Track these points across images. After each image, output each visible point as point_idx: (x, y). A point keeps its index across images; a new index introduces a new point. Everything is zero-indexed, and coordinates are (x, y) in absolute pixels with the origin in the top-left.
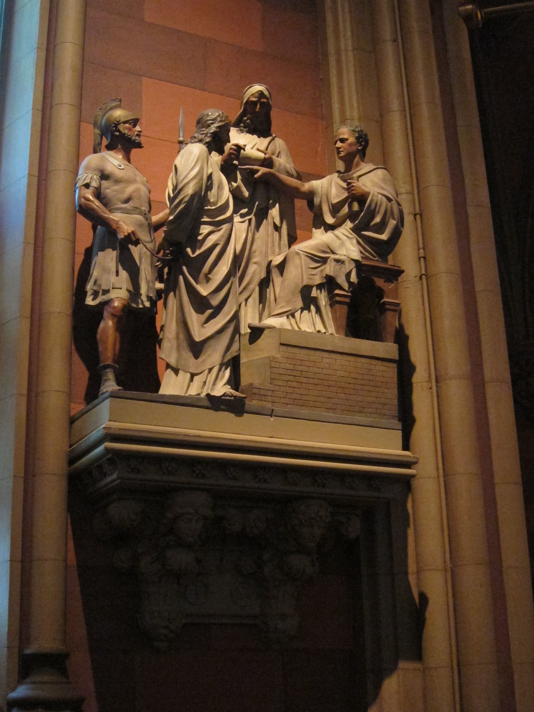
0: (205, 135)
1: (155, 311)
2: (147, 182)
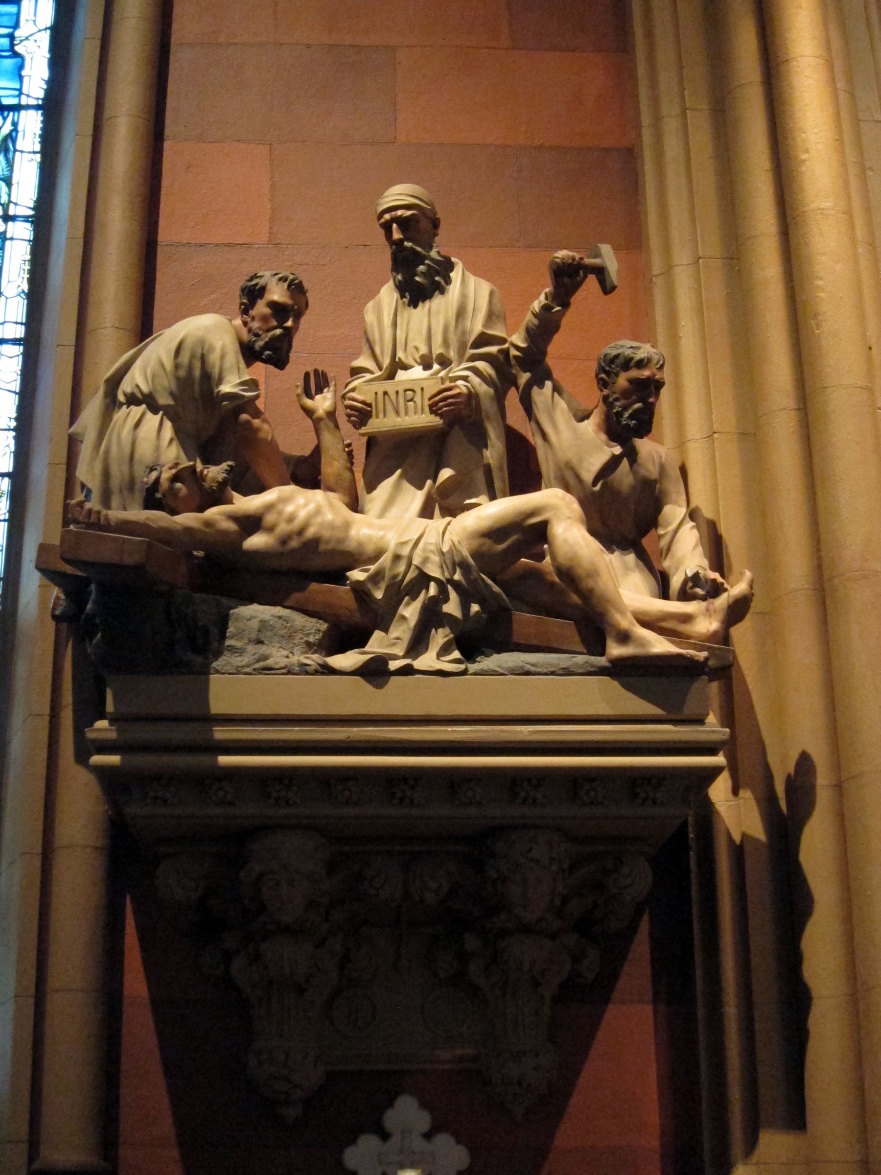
0: (396, 406)
1: (468, 501)
2: (29, 14)
